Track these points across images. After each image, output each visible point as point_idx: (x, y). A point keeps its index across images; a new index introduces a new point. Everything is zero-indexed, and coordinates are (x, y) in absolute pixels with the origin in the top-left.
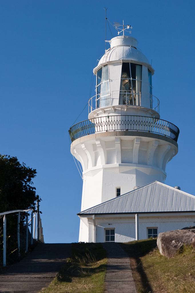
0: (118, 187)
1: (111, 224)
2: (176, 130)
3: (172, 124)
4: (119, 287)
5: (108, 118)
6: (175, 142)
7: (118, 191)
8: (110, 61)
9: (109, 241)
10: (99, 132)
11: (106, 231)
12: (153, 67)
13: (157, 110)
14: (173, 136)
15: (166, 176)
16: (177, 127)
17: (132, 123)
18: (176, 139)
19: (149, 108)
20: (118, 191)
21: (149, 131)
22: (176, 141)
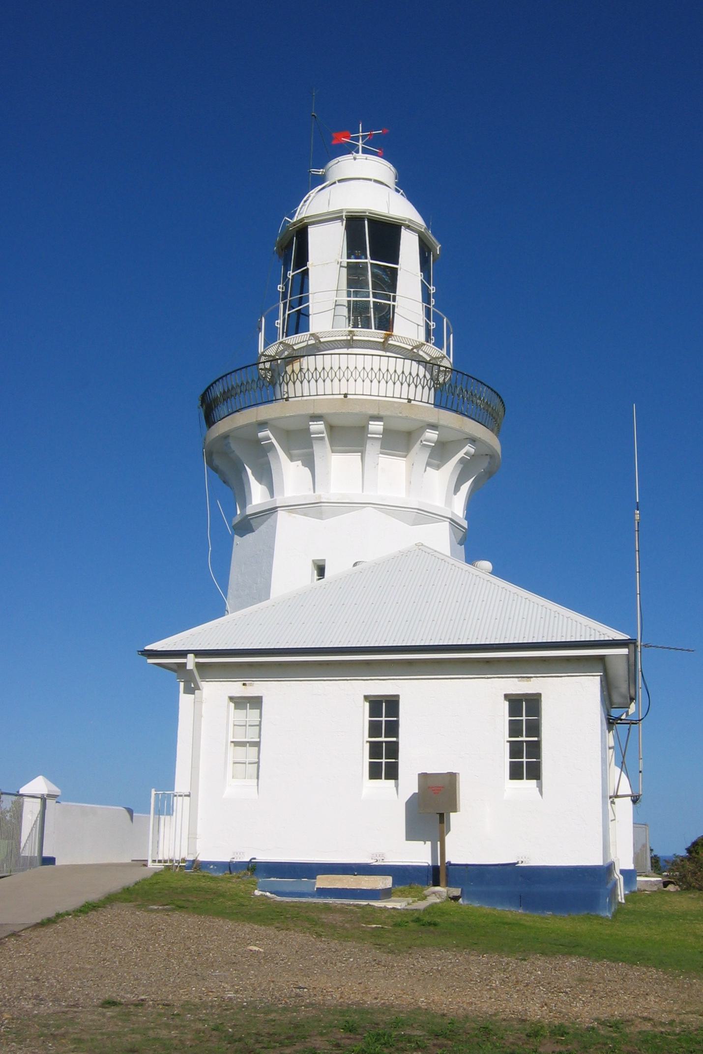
7: (321, 570)
11: (371, 703)
20: (321, 570)
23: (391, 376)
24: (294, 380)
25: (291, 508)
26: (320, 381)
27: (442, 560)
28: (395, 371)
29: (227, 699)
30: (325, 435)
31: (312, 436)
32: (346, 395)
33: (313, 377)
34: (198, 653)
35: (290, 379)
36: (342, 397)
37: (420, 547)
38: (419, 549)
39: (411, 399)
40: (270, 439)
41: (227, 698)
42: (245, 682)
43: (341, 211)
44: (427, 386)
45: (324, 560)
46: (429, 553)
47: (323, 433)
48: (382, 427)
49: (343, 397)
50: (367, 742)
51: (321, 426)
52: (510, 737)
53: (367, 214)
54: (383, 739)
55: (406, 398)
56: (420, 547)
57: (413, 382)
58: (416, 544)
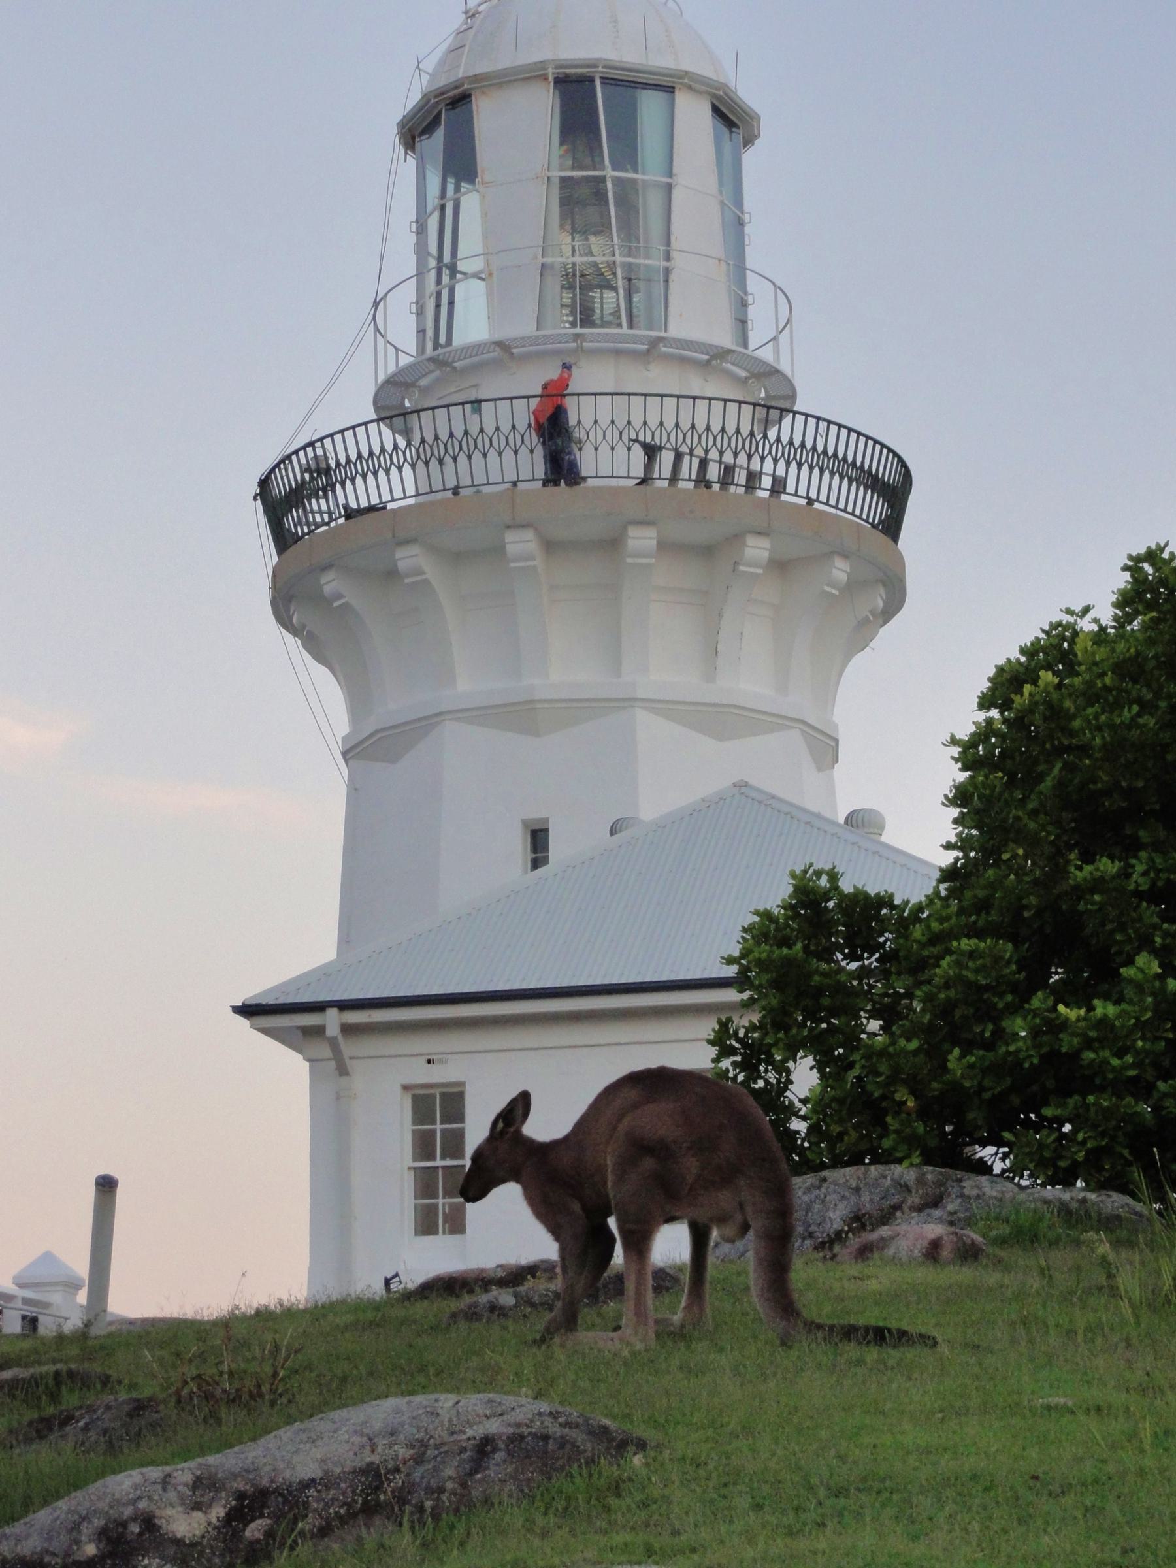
0: (535, 813)
1: (444, 1062)
2: (888, 473)
3: (876, 442)
4: (997, 790)
5: (478, 411)
6: (891, 542)
7: (538, 839)
8: (748, 272)
9: (434, 1159)
10: (439, 496)
11: (416, 1100)
12: (749, 94)
13: (766, 354)
14: (873, 506)
15: (837, 741)
16: (896, 454)
17: (600, 437)
18: (891, 527)
19: (724, 338)
20: (538, 839)
21: (810, 502)
22: (895, 538)
23: (669, 435)
24: (361, 462)
25: (654, 705)
26: (477, 457)
27: (787, 814)
28: (677, 425)
29: (399, 1090)
30: (537, 563)
31: (512, 565)
32: (515, 484)
33: (445, 445)
34: (344, 1006)
35: (461, 448)
36: (449, 494)
37: (743, 790)
38: (742, 794)
39: (711, 480)
40: (423, 573)
41: (400, 1088)
42: (429, 1057)
43: (543, 64)
44: (784, 444)
45: (547, 820)
46: (760, 802)
47: (533, 558)
48: (655, 542)
49: (452, 496)
50: (409, 1168)
51: (530, 544)
52: (414, 1160)
53: (433, 101)
54: (438, 1163)
55: (764, 471)
56: (743, 790)
57: (715, 444)
58: (734, 785)
